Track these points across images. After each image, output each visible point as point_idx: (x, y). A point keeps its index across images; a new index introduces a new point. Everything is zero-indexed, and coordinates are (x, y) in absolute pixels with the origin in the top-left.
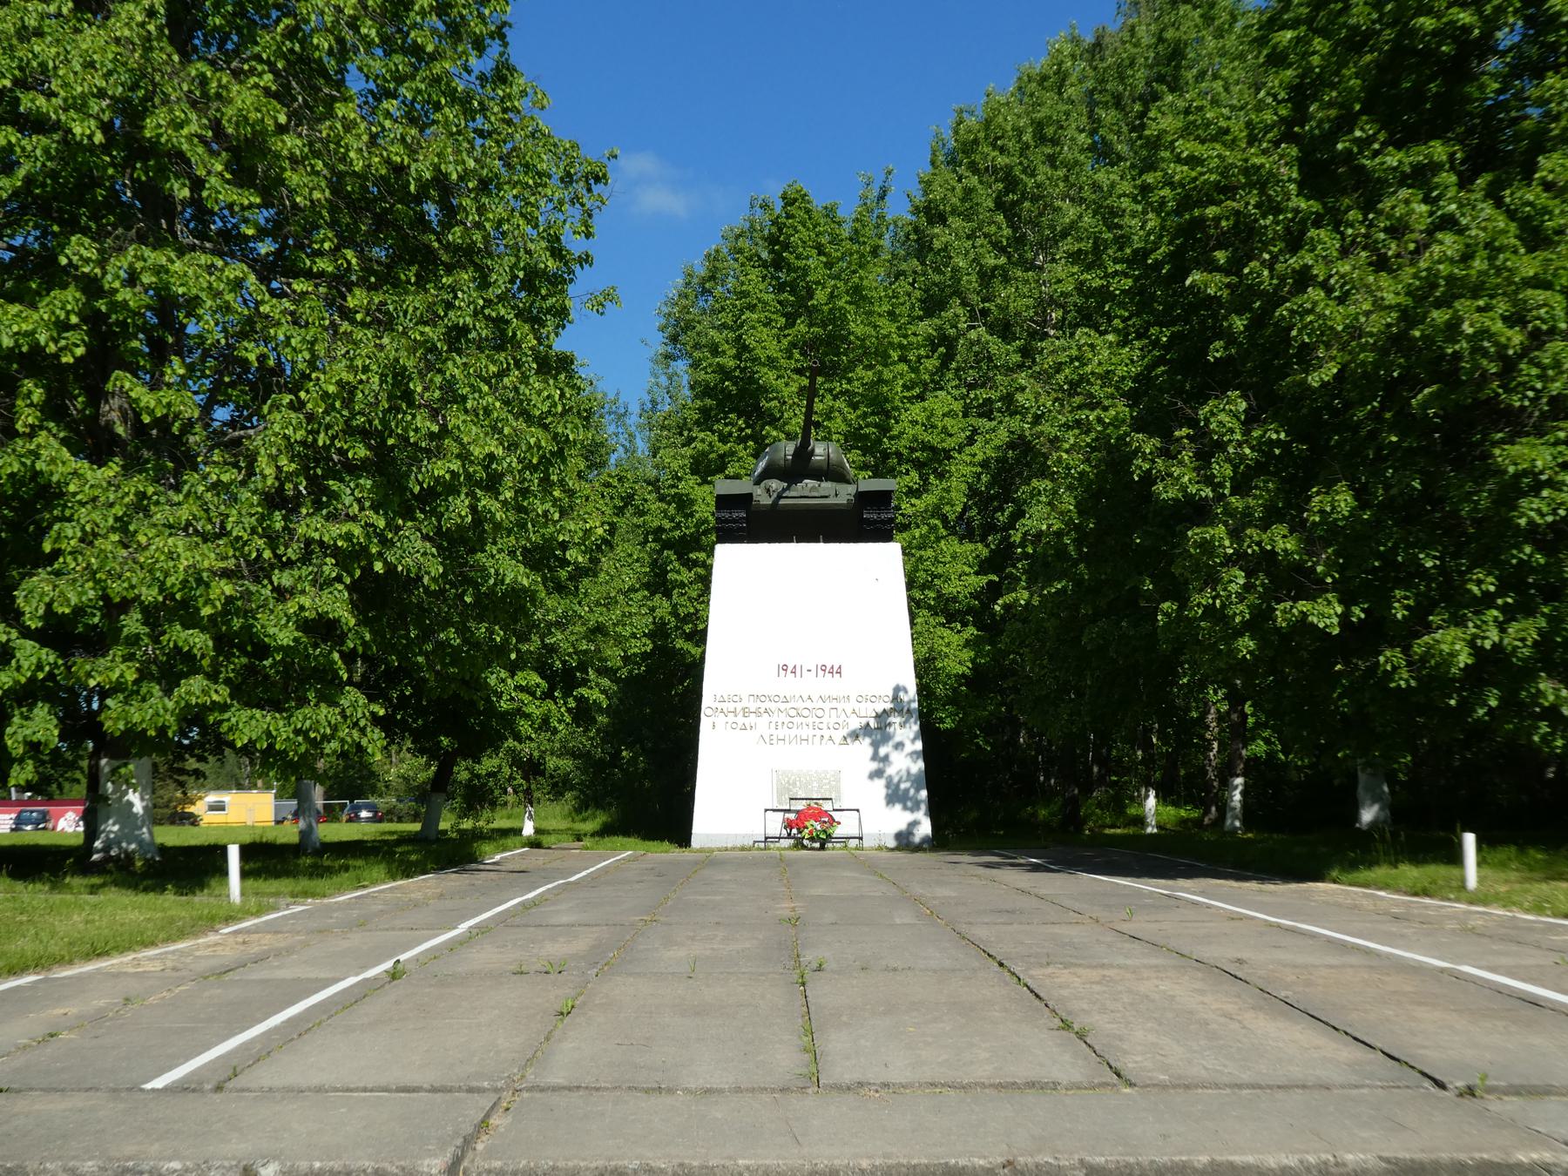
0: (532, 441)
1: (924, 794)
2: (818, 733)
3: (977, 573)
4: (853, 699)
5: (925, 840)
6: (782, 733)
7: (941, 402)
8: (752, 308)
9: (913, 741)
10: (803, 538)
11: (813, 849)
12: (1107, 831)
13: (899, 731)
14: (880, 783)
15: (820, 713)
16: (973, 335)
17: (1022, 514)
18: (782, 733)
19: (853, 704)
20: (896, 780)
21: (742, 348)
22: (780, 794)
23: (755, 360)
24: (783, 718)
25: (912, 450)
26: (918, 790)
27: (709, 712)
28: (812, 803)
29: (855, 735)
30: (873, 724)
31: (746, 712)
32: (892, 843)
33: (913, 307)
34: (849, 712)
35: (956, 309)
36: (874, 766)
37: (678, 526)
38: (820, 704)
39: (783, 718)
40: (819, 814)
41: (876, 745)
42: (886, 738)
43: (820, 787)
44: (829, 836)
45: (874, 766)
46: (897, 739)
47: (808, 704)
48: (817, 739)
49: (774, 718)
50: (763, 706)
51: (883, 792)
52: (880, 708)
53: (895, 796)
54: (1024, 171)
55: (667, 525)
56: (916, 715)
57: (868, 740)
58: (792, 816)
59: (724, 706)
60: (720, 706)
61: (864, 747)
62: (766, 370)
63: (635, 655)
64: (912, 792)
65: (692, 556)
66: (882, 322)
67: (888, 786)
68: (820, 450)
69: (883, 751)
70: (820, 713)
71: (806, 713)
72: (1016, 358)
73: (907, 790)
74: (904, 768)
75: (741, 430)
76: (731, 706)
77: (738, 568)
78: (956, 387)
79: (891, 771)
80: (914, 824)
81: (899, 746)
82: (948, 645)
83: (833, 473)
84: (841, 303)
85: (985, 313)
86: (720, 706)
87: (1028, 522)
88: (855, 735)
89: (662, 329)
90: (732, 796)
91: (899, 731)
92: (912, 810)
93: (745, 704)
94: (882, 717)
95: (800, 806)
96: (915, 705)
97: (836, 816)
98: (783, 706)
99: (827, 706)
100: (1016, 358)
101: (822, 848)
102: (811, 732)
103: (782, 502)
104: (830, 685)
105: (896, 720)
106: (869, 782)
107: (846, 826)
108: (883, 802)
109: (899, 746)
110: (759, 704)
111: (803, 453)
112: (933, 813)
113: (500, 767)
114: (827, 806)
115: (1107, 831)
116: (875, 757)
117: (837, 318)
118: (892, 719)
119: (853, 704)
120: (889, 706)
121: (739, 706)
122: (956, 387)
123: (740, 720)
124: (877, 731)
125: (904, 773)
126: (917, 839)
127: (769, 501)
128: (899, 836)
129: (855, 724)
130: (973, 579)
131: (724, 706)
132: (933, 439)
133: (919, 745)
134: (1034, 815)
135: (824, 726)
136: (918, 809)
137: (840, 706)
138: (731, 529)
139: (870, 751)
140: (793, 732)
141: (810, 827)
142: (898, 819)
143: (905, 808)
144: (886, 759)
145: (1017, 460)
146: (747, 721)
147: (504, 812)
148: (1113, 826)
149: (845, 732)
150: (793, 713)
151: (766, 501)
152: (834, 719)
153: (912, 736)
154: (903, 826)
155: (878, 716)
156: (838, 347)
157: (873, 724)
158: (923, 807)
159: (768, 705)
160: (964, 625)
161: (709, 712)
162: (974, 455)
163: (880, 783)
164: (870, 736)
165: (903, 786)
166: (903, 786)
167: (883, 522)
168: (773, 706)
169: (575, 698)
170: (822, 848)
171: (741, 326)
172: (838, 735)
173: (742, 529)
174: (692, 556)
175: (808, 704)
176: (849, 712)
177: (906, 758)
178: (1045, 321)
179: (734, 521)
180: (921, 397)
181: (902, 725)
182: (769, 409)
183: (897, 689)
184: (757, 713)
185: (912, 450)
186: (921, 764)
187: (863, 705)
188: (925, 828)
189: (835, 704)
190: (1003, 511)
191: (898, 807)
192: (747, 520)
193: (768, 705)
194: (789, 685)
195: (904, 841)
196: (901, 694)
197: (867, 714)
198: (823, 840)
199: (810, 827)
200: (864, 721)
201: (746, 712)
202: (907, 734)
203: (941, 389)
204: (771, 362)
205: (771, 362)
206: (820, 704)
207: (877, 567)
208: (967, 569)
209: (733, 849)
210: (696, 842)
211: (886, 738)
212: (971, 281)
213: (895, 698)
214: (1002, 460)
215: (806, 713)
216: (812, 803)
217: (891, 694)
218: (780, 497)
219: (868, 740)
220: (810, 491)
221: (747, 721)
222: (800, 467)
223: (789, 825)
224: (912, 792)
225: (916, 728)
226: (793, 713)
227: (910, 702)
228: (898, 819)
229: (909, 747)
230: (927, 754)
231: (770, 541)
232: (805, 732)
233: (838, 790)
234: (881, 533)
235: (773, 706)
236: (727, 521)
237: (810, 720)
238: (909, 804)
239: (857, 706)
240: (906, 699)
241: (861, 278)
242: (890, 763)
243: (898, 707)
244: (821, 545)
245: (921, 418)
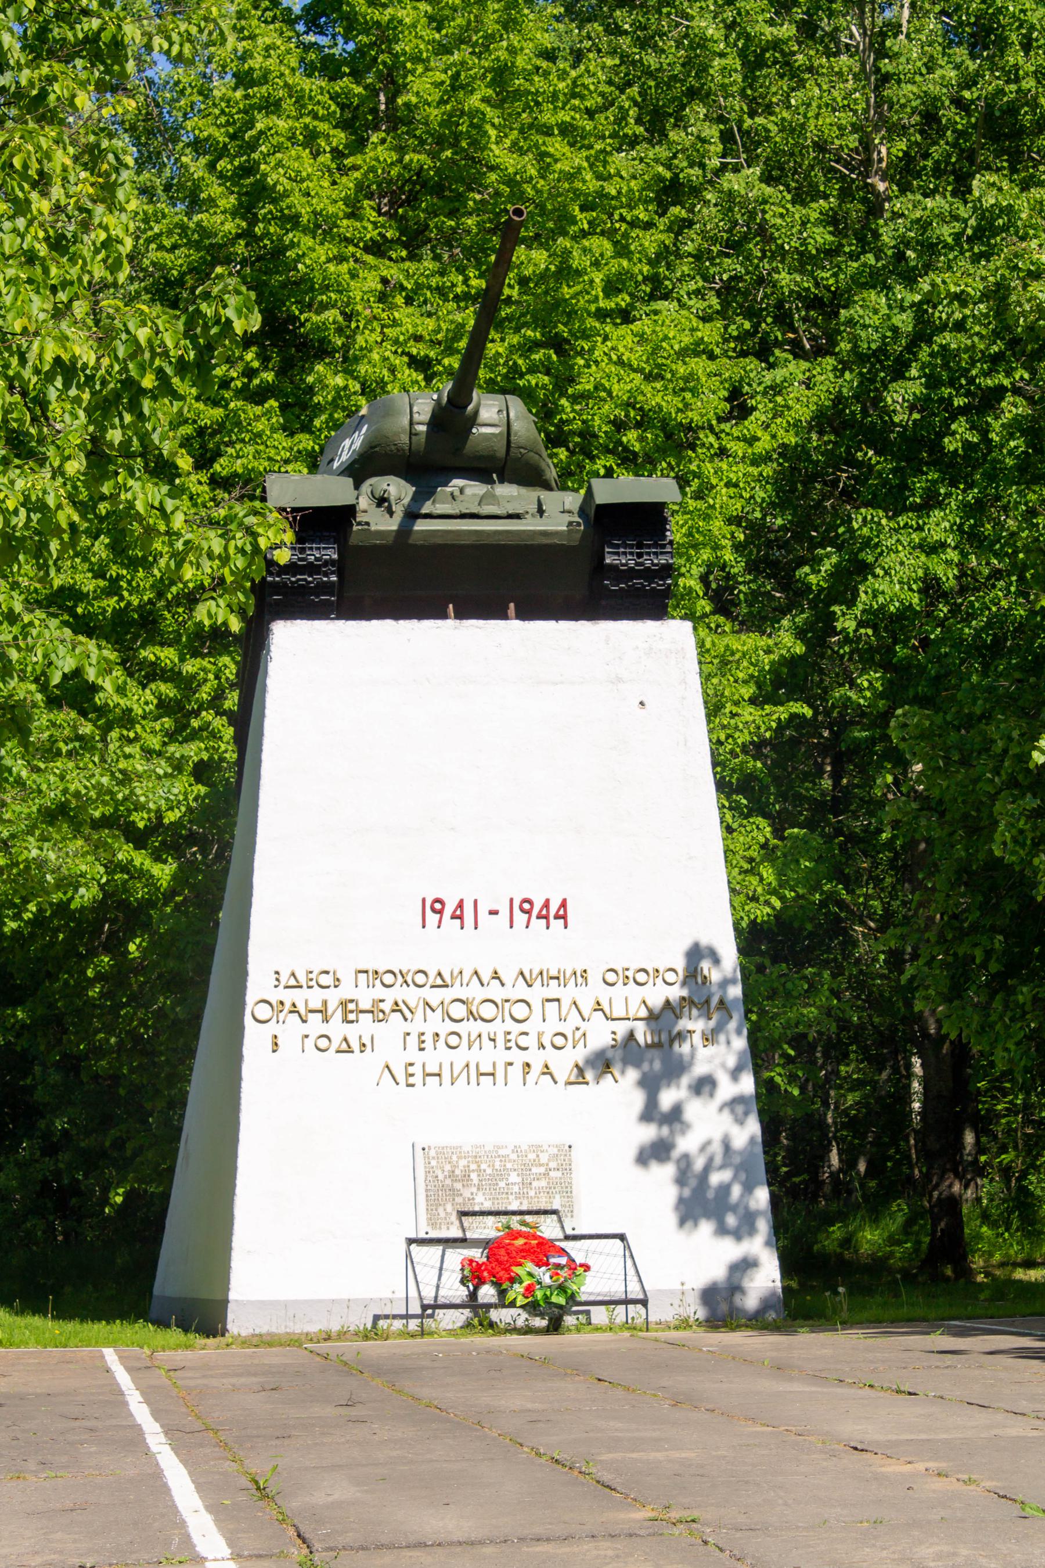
0: (143, 334)
1: (762, 1196)
2: (518, 1057)
4: (595, 978)
5: (767, 1304)
6: (435, 1057)
7: (675, 322)
8: (271, 106)
9: (735, 1074)
10: (532, 609)
11: (528, 1330)
13: (704, 1053)
14: (664, 1173)
15: (520, 1011)
16: (732, 182)
17: (864, 569)
18: (435, 1057)
19: (595, 989)
20: (699, 1164)
21: (254, 196)
22: (433, 1204)
23: (292, 221)
24: (435, 1023)
25: (619, 426)
26: (749, 1188)
27: (263, 1011)
28: (515, 1222)
29: (602, 1063)
30: (642, 1034)
31: (349, 1010)
33: (621, 119)
35: (699, 124)
36: (649, 1133)
37: (113, 589)
38: (521, 991)
40: (541, 1251)
41: (650, 1085)
42: (675, 1069)
43: (526, 1184)
44: (572, 1299)
45: (649, 1133)
46: (700, 1069)
47: (495, 991)
49: (416, 1026)
50: (390, 996)
51: (671, 1193)
52: (657, 995)
53: (698, 1203)
55: (90, 585)
56: (737, 1016)
57: (632, 1075)
58: (477, 1254)
59: (298, 997)
60: (289, 997)
61: (623, 1090)
62: (307, 241)
64: (736, 1191)
65: (148, 654)
66: (556, 146)
67: (681, 1180)
68: (492, 414)
69: (667, 1098)
70: (520, 1011)
71: (488, 1011)
73: (724, 1189)
74: (717, 1137)
75: (250, 373)
77: (322, 672)
78: (698, 293)
79: (687, 1144)
80: (745, 1265)
81: (704, 1086)
83: (507, 466)
84: (474, 101)
85: (753, 141)
87: (882, 585)
88: (602, 1063)
91: (704, 1053)
92: (738, 1235)
93: (346, 991)
95: (488, 1229)
96: (735, 991)
97: (577, 1251)
98: (435, 997)
99: (536, 994)
100: (821, 236)
101: (555, 1326)
102: (502, 1056)
103: (420, 526)
105: (695, 1025)
106: (638, 1171)
107: (602, 1275)
108: (671, 1218)
109: (704, 1086)
110: (379, 992)
114: (549, 1229)
115: (1020, 1274)
116: (650, 1113)
117: (460, 138)
119: (595, 989)
120: (676, 993)
121: (333, 998)
122: (698, 293)
123: (336, 1028)
124: (651, 1053)
125: (717, 1148)
126: (751, 1302)
127: (392, 525)
128: (709, 1295)
129: (601, 1035)
130: (749, 713)
131: (298, 997)
132: (656, 397)
133: (747, 1084)
134: (847, 1242)
136: (752, 1231)
137: (567, 993)
138: (303, 590)
139: (638, 1099)
140: (460, 1056)
142: (704, 1256)
143: (722, 1230)
144: (675, 1117)
146: (353, 1032)
148: (1029, 1264)
149: (579, 1054)
150: (458, 1011)
151: (385, 524)
152: (553, 1025)
153: (732, 1062)
154: (716, 1271)
155: (652, 1017)
156: (460, 198)
157: (642, 1034)
158: (763, 1226)
159: (400, 993)
161: (263, 1011)
162: (752, 440)
163: (664, 1173)
164: (637, 1065)
165: (716, 1178)
166: (716, 1178)
167: (649, 574)
168: (411, 995)
170: (555, 1326)
171: (252, 146)
172: (564, 1063)
173: (324, 588)
174: (148, 654)
175: (495, 991)
177: (720, 1122)
178: (868, 162)
180: (626, 316)
181: (710, 1038)
182: (322, 327)
183: (696, 954)
184: (376, 1012)
185: (619, 426)
186: (753, 1127)
188: (767, 1277)
189: (553, 990)
190: (815, 562)
191: (706, 1227)
192: (339, 566)
193: (400, 993)
194: (446, 948)
195: (721, 1306)
196: (705, 965)
198: (554, 1314)
200: (622, 1029)
201: (349, 1010)
202: (720, 1054)
203: (666, 297)
204: (322, 227)
205: (322, 227)
206: (521, 991)
209: (342, 1335)
210: (238, 1323)
211: (675, 1069)
212: (725, 67)
213: (692, 975)
215: (488, 1011)
216: (515, 1222)
217: (680, 965)
218: (412, 515)
219: (632, 1075)
220: (468, 509)
221: (353, 1032)
222: (443, 453)
223: (474, 1275)
224: (736, 1191)
225: (740, 1043)
226: (458, 1011)
227: (725, 983)
228: (704, 1256)
229: (726, 1089)
230: (768, 1103)
232: (487, 1056)
233: (567, 1191)
234: (645, 598)
235: (411, 995)
237: (498, 1028)
238: (731, 1220)
239: (604, 994)
240: (715, 976)
241: (512, 51)
242: (685, 1127)
243: (698, 995)
244: (515, 625)
245: (637, 356)
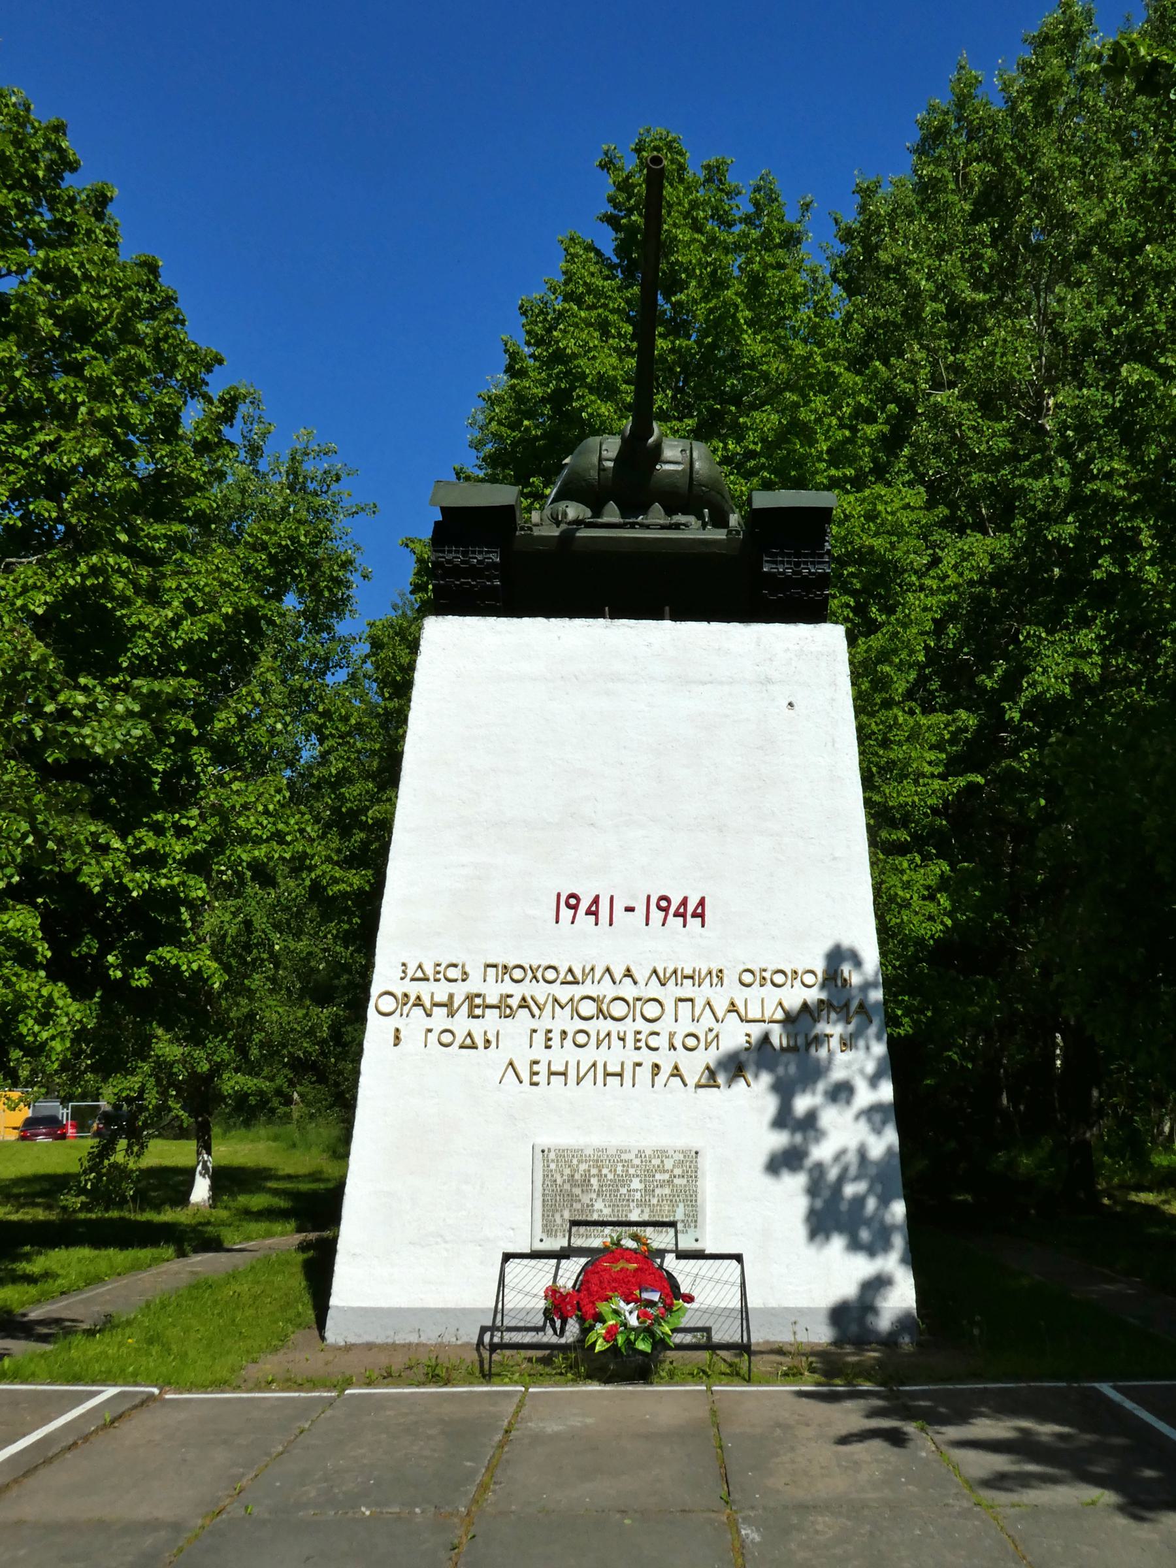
1: (899, 1209)
3: (943, 777)
4: (730, 977)
6: (561, 1056)
9: (874, 1081)
12: (1133, 1197)
13: (841, 1058)
14: (794, 1183)
15: (652, 1010)
18: (561, 1056)
19: (731, 990)
20: (833, 1174)
22: (549, 1208)
24: (564, 1020)
27: (387, 1004)
29: (735, 1066)
30: (778, 1037)
31: (475, 1005)
32: (822, 1335)
34: (721, 1008)
36: (780, 1140)
39: (564, 1020)
41: (785, 1091)
42: (811, 1073)
44: (660, 1344)
45: (780, 1140)
46: (838, 1074)
47: (628, 990)
48: (644, 1073)
49: (545, 1023)
50: (518, 991)
51: (800, 1204)
52: (796, 997)
53: (828, 1217)
54: (1020, 159)
57: (766, 1079)
59: (424, 990)
60: (414, 989)
63: (345, 895)
64: (871, 1204)
67: (813, 1190)
69: (802, 1104)
70: (652, 1010)
71: (618, 1009)
72: (1004, 444)
73: (859, 1201)
76: (441, 992)
79: (822, 1152)
81: (841, 1092)
82: (907, 886)
86: (414, 989)
88: (735, 1066)
89: (477, 445)
90: (433, 1217)
91: (841, 1058)
93: (474, 985)
94: (800, 1021)
98: (564, 993)
104: (679, 945)
106: (767, 1181)
107: (708, 1291)
108: (800, 1231)
110: (508, 987)
111: (639, 454)
112: (916, 1260)
113: (142, 1090)
116: (783, 1119)
118: (823, 1028)
119: (731, 990)
120: (814, 995)
121: (460, 991)
123: (462, 1024)
124: (785, 1058)
125: (852, 1158)
128: (840, 1314)
131: (424, 990)
133: (886, 1092)
135: (661, 1042)
137: (701, 994)
139: (771, 1104)
140: (588, 1056)
141: (614, 1306)
142: (839, 1272)
143: (855, 1245)
144: (809, 1124)
145: (1005, 602)
146: (477, 1028)
147: (274, 1130)
149: (710, 1057)
150: (587, 1008)
152: (685, 1026)
153: (870, 1068)
155: (790, 1020)
157: (778, 1037)
158: (899, 1242)
159: (528, 989)
160: (926, 857)
163: (794, 1183)
164: (771, 1069)
165: (850, 1190)
166: (850, 1190)
168: (540, 991)
169: (153, 969)
172: (695, 1064)
175: (628, 990)
176: (721, 1008)
177: (855, 1130)
179: (474, 572)
181: (847, 1043)
183: (838, 957)
184: (504, 1007)
186: (891, 1137)
187: (756, 992)
189: (688, 990)
191: (838, 1243)
193: (528, 989)
196: (846, 969)
197: (770, 1004)
199: (614, 1306)
200: (756, 1031)
201: (475, 1005)
202: (858, 1061)
207: (792, 679)
208: (927, 769)
211: (811, 1073)
213: (832, 978)
214: (980, 602)
215: (618, 1009)
217: (819, 966)
219: (766, 1079)
221: (477, 1028)
224: (871, 1204)
225: (880, 1049)
226: (587, 1008)
227: (866, 986)
228: (839, 1272)
229: (865, 1096)
230: (906, 1113)
231: (548, 615)
232: (615, 1056)
233: (691, 1198)
235: (540, 991)
236: (455, 571)
237: (629, 1027)
238: (865, 1235)
239: (740, 995)
240: (856, 979)
244: (667, 624)
